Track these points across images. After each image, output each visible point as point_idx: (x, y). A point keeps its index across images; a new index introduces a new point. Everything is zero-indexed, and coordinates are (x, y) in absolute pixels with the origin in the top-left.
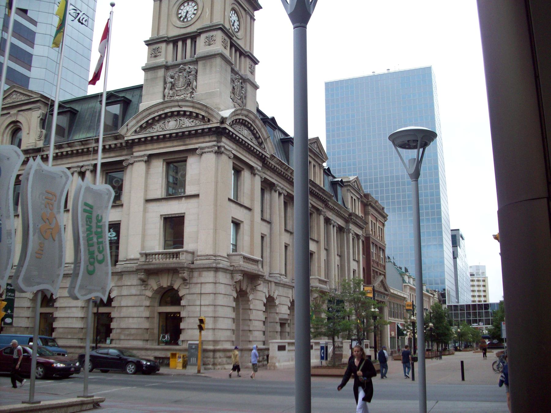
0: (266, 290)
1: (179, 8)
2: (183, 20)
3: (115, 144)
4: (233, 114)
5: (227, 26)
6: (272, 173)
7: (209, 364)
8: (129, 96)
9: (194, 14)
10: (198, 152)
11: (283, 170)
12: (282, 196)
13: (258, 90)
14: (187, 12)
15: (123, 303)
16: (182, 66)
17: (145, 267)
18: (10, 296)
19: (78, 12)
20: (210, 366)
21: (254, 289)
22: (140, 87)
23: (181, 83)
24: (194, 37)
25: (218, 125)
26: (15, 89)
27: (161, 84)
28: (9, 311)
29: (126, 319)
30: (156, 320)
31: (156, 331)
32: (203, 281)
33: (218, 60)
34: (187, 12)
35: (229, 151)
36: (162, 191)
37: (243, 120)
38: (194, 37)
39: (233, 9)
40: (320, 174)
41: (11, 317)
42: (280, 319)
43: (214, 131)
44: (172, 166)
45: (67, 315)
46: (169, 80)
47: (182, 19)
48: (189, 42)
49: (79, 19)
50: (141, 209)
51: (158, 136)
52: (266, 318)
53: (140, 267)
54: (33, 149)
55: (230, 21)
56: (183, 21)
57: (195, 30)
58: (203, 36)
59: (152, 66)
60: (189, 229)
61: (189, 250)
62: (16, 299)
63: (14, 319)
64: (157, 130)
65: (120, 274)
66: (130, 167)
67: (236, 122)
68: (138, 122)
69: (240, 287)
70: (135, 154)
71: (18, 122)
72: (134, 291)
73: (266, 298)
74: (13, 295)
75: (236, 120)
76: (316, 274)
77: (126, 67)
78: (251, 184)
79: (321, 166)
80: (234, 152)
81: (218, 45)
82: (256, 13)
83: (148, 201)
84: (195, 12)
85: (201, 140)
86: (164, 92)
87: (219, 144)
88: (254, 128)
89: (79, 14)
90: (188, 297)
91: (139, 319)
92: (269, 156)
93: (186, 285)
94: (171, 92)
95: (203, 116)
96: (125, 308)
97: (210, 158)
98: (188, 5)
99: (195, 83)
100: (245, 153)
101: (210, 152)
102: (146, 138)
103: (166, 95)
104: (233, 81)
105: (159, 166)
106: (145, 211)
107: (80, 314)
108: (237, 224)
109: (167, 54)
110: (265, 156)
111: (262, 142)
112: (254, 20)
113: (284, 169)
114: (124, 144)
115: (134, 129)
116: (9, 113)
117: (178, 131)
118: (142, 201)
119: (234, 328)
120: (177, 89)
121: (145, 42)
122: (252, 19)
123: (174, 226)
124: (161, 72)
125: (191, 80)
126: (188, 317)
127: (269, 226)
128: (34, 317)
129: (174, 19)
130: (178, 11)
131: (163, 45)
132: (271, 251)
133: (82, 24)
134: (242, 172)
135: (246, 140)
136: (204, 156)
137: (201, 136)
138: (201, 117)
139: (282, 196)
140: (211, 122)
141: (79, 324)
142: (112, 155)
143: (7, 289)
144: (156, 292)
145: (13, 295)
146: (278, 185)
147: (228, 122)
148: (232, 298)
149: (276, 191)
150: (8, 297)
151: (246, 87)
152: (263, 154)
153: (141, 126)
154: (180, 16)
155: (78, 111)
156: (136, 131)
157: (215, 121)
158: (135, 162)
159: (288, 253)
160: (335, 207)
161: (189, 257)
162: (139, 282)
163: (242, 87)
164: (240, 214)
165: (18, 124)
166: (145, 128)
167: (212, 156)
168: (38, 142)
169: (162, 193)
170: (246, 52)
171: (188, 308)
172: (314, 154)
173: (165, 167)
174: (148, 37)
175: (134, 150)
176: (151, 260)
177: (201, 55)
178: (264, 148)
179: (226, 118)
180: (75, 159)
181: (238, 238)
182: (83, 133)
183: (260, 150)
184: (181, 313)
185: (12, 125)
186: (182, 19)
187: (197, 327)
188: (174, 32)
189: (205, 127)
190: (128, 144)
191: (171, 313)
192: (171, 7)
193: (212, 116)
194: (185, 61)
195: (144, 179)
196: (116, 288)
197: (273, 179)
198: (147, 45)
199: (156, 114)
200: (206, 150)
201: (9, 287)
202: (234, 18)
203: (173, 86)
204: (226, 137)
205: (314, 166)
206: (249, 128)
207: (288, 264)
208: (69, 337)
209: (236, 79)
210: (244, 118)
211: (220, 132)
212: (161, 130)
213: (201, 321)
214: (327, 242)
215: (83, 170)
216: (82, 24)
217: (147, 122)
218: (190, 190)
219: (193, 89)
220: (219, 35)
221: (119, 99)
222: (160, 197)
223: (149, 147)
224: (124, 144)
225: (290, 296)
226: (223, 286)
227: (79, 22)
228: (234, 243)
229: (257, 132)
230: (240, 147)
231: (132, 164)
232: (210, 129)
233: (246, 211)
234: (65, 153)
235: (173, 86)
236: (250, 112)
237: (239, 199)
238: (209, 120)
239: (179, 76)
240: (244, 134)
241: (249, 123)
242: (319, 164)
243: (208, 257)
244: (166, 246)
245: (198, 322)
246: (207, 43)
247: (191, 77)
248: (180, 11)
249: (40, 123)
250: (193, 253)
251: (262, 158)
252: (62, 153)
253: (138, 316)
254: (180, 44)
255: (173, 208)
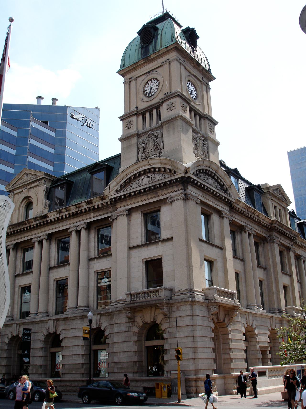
0: (244, 321)
1: (145, 87)
2: (149, 95)
3: (102, 204)
4: (196, 165)
5: (184, 93)
6: (240, 217)
7: (192, 393)
8: (111, 164)
9: (157, 89)
10: (169, 201)
11: (249, 213)
12: (252, 237)
13: (219, 147)
14: (151, 88)
15: (115, 340)
16: (150, 132)
17: (132, 305)
18: (26, 339)
19: (86, 118)
20: (193, 395)
21: (230, 319)
22: (118, 156)
23: (151, 146)
24: (157, 107)
25: (183, 175)
26: (25, 172)
27: (135, 149)
28: (26, 352)
29: (119, 354)
30: (144, 354)
31: (144, 364)
32: (181, 315)
33: (180, 122)
34: (151, 88)
35: (196, 197)
36: (142, 238)
37: (206, 170)
38: (157, 107)
39: (189, 81)
40: (286, 216)
41: (29, 357)
42: (260, 347)
43: (180, 181)
44: (149, 216)
45: (71, 354)
46: (141, 145)
47: (147, 95)
48: (154, 112)
49: (87, 124)
50: (126, 255)
51: (135, 192)
52: (246, 347)
53: (126, 306)
54: (40, 217)
55: (187, 91)
56: (149, 96)
57: (158, 101)
58: (165, 104)
59: (127, 136)
60: (166, 269)
61: (167, 288)
62: (32, 341)
63: (31, 358)
64: (134, 187)
65: (111, 315)
66: (115, 222)
67: (200, 172)
68: (118, 183)
69: (217, 318)
70: (118, 210)
71: (29, 197)
72: (123, 329)
73: (245, 328)
74: (29, 338)
75: (200, 170)
76: (292, 304)
77: (109, 144)
78: (221, 227)
79: (285, 209)
80: (200, 198)
81: (179, 109)
82: (211, 84)
83: (131, 248)
84: (157, 87)
85: (170, 190)
86: (138, 156)
87: (186, 192)
88: (218, 177)
89: (86, 120)
90: (170, 330)
91: (129, 353)
92: (234, 201)
93: (167, 320)
94: (143, 155)
95: (170, 170)
96: (116, 344)
97: (179, 204)
98: (151, 82)
99: (162, 144)
100: (211, 199)
101: (178, 199)
102: (125, 195)
103: (140, 158)
104: (194, 139)
105: (138, 219)
106: (129, 257)
107: (82, 352)
108: (211, 263)
109: (138, 124)
110: (231, 201)
111: (227, 189)
112: (210, 89)
113: (251, 212)
114: (109, 203)
115: (115, 189)
116: (22, 191)
117: (150, 185)
118: (126, 249)
119: (214, 357)
120: (148, 152)
121: (120, 118)
122: (208, 88)
123: (154, 268)
124: (134, 140)
125: (159, 143)
126: (171, 349)
127: (242, 263)
128: (46, 357)
129: (142, 96)
130: (144, 89)
131: (134, 118)
132: (246, 286)
133: (90, 127)
134: (211, 216)
135: (211, 187)
136: (174, 203)
137: (170, 187)
138: (168, 170)
139: (252, 237)
140: (177, 174)
141: (81, 361)
142: (101, 213)
143: (24, 333)
144: (142, 328)
145: (29, 338)
146: (246, 226)
147: (192, 172)
148: (210, 330)
149: (245, 232)
150: (24, 340)
151: (208, 144)
152: (228, 199)
153: (121, 186)
154: (145, 92)
155: (73, 182)
156: (117, 191)
157: (180, 172)
158: (118, 216)
159: (264, 287)
160: (303, 244)
161: (168, 294)
162: (127, 320)
163: (204, 145)
164: (213, 253)
165: (30, 199)
166: (124, 187)
167: (181, 202)
168: (44, 211)
169: (142, 240)
170: (205, 115)
171: (171, 341)
172: (278, 199)
173: (143, 217)
174: (122, 113)
175: (117, 207)
176: (135, 299)
177: (164, 120)
178: (229, 194)
179: (189, 168)
180: (72, 221)
181: (213, 274)
182: (77, 199)
183: (226, 196)
184: (164, 346)
185: (25, 200)
186: (147, 95)
187: (175, 358)
188: (142, 106)
189: (172, 178)
190: (112, 203)
191: (156, 346)
192: (138, 87)
193: (178, 169)
194: (153, 127)
195: (127, 230)
196: (109, 327)
197: (242, 221)
198: (121, 120)
199: (132, 174)
200: (175, 198)
201: (25, 332)
202: (191, 88)
203: (145, 149)
204: (191, 185)
205: (280, 210)
206: (213, 178)
207: (264, 296)
208: (74, 372)
209: (197, 138)
210: (207, 168)
211: (185, 181)
212: (137, 186)
213: (178, 352)
214: (300, 276)
215: (79, 228)
216: (90, 127)
217: (125, 182)
218: (164, 235)
219: (161, 149)
220: (178, 101)
221: (103, 167)
222: (140, 243)
223: (129, 202)
224: (109, 203)
225: (269, 325)
226: (200, 318)
227: (88, 126)
228: (210, 280)
229: (221, 180)
230: (206, 194)
231: (116, 218)
232: (176, 179)
233: (219, 250)
234: (64, 217)
235: (145, 149)
236: (211, 162)
237: (210, 240)
238: (175, 172)
239: (148, 141)
240: (209, 183)
241: (212, 172)
242: (284, 208)
243: (184, 292)
244: (148, 286)
245: (175, 352)
246: (169, 110)
247: (158, 140)
248: (145, 89)
249: (45, 195)
250: (171, 290)
251: (229, 204)
252: (62, 216)
253: (128, 350)
254: (147, 115)
255: (152, 252)
